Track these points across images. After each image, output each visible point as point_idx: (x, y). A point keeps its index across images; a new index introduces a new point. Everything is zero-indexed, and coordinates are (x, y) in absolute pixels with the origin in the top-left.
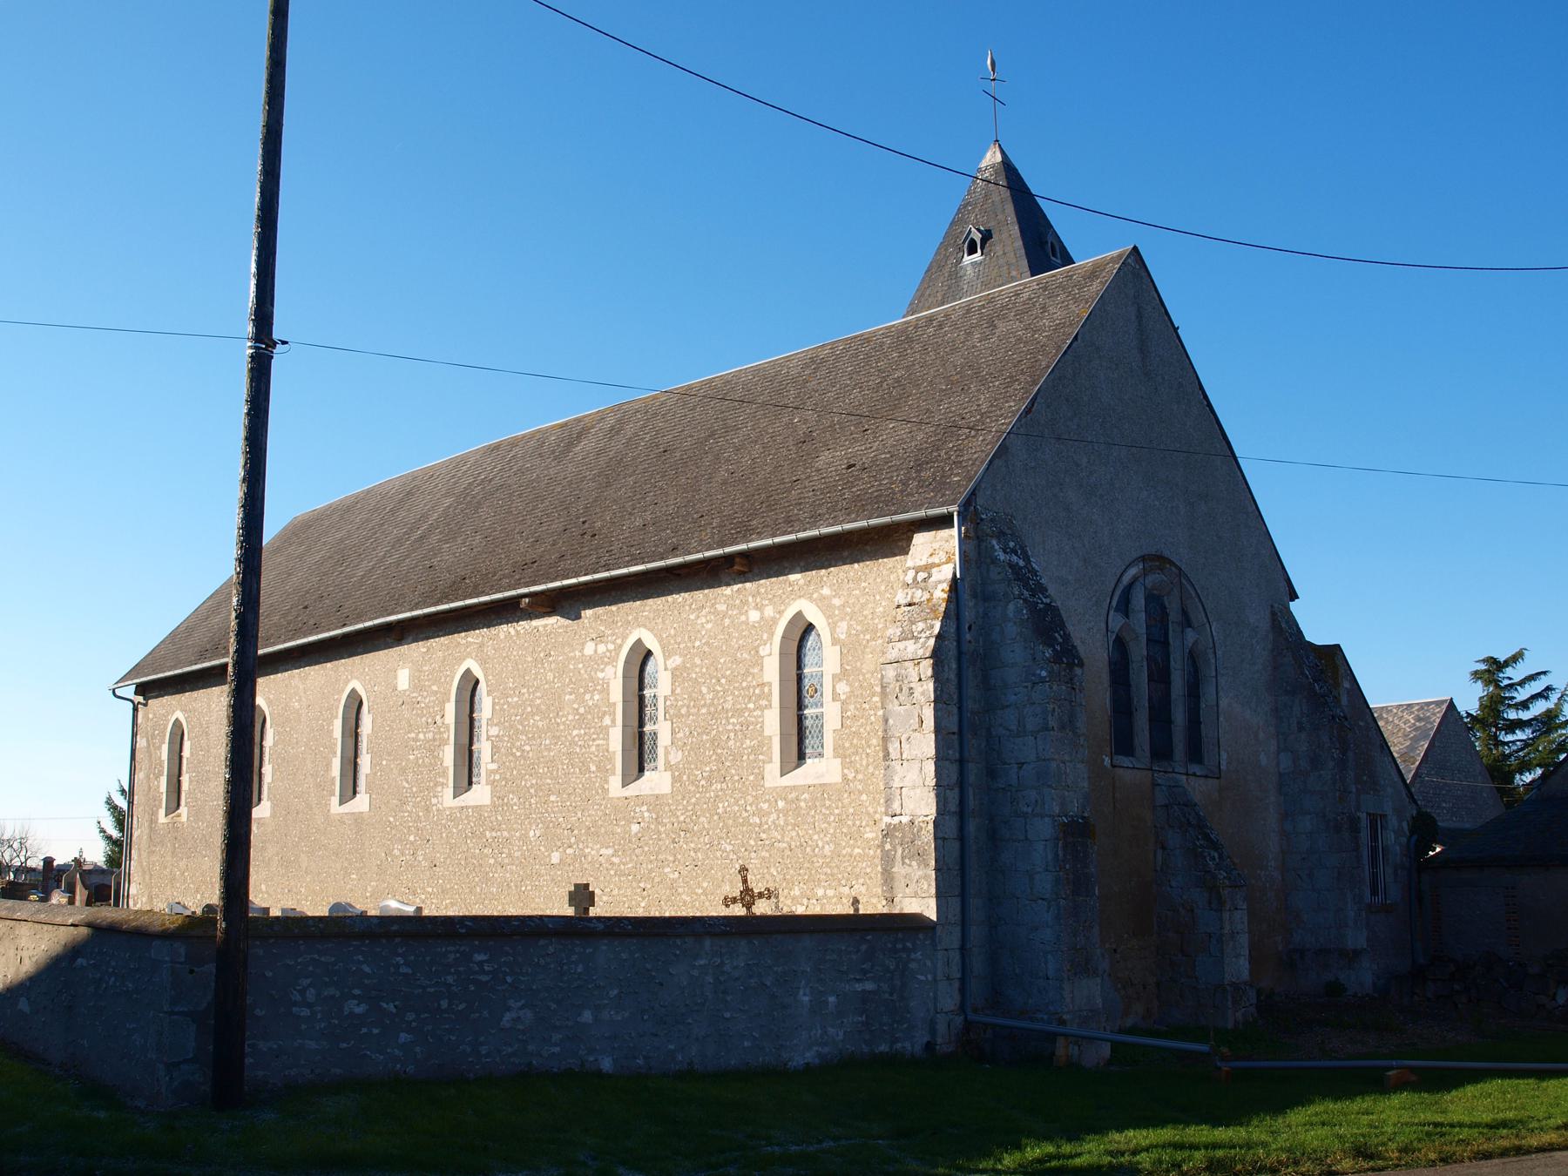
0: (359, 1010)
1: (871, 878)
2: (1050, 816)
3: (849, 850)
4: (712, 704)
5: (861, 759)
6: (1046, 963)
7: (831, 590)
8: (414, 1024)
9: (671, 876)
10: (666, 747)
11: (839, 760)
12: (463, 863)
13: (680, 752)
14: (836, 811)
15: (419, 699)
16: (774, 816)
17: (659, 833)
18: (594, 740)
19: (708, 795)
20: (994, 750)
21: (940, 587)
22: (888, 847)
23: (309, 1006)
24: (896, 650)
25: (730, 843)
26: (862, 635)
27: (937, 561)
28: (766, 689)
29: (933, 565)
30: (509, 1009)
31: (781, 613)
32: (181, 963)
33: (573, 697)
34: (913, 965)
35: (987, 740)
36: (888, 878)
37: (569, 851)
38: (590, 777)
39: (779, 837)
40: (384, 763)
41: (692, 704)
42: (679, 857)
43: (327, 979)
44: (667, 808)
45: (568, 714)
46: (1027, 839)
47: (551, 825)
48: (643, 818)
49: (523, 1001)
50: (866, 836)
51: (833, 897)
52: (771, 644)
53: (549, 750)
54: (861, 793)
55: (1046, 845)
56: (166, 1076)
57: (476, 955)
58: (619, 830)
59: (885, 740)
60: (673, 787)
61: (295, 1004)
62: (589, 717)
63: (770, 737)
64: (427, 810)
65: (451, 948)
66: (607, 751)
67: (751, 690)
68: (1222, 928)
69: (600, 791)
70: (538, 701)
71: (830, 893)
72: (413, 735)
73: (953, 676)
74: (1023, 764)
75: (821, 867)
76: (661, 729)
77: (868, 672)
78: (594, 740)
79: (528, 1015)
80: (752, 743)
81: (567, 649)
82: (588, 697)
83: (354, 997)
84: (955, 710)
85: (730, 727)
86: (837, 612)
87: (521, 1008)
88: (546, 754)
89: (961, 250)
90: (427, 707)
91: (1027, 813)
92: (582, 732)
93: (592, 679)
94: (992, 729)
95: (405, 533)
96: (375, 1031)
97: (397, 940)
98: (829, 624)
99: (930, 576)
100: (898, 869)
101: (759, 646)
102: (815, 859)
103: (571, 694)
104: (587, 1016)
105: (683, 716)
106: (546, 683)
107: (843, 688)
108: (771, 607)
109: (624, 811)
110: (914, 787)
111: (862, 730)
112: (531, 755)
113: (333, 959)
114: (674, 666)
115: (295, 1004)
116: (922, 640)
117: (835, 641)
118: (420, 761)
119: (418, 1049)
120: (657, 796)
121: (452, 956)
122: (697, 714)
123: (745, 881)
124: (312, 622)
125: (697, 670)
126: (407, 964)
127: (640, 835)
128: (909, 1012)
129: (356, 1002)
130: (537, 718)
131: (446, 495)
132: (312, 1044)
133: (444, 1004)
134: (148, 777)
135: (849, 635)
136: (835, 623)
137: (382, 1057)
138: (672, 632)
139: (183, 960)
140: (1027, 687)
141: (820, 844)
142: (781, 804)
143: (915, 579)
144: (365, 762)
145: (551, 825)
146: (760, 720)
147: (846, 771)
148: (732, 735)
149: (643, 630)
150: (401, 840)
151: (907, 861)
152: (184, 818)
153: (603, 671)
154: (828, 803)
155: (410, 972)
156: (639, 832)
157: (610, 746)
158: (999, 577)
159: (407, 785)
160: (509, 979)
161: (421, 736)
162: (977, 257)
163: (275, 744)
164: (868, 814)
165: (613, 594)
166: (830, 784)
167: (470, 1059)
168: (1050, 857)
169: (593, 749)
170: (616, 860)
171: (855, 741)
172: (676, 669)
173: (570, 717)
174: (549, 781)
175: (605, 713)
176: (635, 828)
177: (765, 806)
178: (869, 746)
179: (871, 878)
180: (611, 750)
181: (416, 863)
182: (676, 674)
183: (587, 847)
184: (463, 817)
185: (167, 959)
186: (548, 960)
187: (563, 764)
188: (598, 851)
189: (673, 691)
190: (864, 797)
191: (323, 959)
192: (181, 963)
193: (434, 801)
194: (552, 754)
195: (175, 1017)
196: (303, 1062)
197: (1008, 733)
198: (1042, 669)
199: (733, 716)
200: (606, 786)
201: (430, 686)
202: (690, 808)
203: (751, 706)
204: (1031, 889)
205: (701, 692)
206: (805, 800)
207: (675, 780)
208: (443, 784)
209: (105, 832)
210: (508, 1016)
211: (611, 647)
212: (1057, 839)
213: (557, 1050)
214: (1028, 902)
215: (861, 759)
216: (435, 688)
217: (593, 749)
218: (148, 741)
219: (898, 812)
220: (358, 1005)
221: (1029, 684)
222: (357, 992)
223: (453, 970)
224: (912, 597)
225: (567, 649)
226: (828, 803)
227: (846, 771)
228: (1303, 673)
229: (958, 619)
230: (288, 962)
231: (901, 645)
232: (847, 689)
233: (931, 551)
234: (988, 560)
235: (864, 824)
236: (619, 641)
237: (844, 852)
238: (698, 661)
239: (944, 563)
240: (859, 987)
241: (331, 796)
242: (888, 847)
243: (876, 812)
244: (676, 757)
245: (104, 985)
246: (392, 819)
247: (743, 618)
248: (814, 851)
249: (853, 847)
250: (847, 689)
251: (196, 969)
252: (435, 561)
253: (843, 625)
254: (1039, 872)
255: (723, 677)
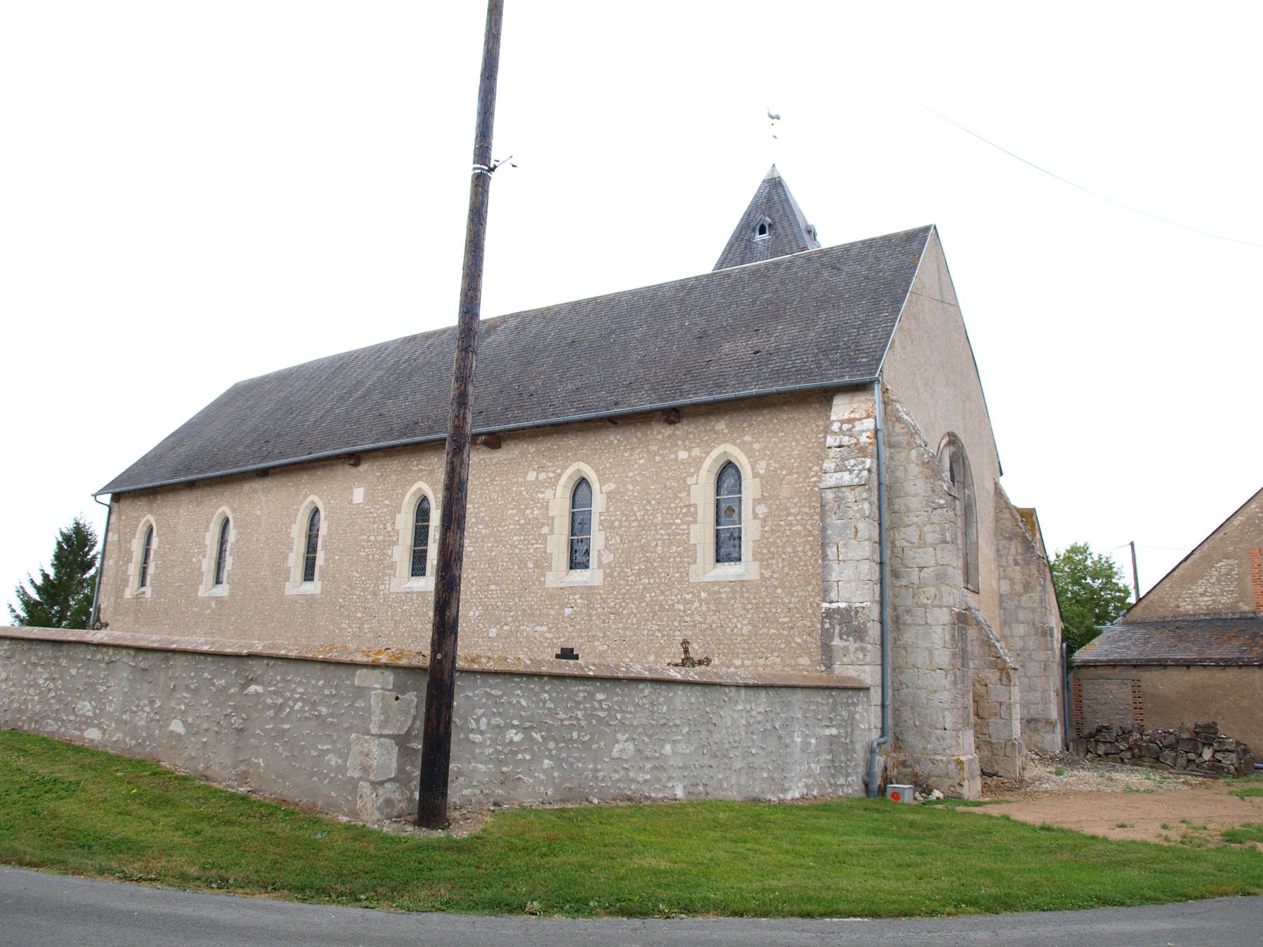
0: (517, 738)
1: (784, 652)
2: (947, 607)
3: (766, 630)
4: (643, 519)
5: (777, 563)
6: (944, 718)
7: (753, 438)
8: (554, 752)
9: (601, 648)
10: (599, 551)
11: (758, 563)
12: (406, 634)
13: (612, 555)
14: (754, 601)
15: (372, 510)
16: (697, 604)
17: (591, 616)
18: (533, 544)
19: (637, 587)
20: (897, 557)
21: (865, 435)
22: (827, 626)
23: (482, 733)
24: (834, 479)
25: (656, 624)
26: (779, 471)
27: (858, 416)
28: (692, 509)
29: (855, 420)
30: (617, 742)
31: (708, 453)
32: (389, 690)
33: (515, 511)
34: (857, 716)
35: (892, 550)
36: (827, 649)
37: (506, 628)
38: (528, 573)
39: (701, 620)
40: (337, 557)
41: (624, 519)
42: (609, 633)
43: (495, 710)
44: (598, 597)
45: (510, 524)
46: (927, 623)
47: (490, 607)
48: (576, 603)
49: (627, 735)
50: (780, 620)
51: (750, 666)
52: (698, 476)
53: (491, 551)
54: (776, 587)
55: (944, 629)
56: (372, 793)
57: (597, 695)
58: (553, 613)
59: (824, 546)
60: (604, 580)
61: (472, 731)
62: (529, 527)
63: (695, 545)
64: (375, 594)
65: (581, 688)
66: (545, 552)
67: (679, 510)
68: (1010, 698)
69: (537, 583)
70: (482, 514)
71: (747, 663)
72: (365, 537)
73: (876, 501)
74: (923, 568)
75: (739, 643)
76: (597, 539)
77: (784, 498)
78: (533, 544)
79: (630, 747)
80: (679, 549)
81: (510, 476)
82: (528, 511)
83: (514, 727)
84: (877, 526)
85: (659, 537)
86: (757, 454)
87: (626, 740)
88: (488, 553)
89: (754, 230)
90: (379, 516)
91: (927, 604)
92: (522, 538)
93: (532, 498)
94: (896, 542)
95: (346, 393)
96: (528, 757)
97: (546, 679)
98: (750, 462)
99: (854, 427)
100: (836, 642)
101: (686, 477)
102: (734, 637)
103: (513, 509)
104: (668, 748)
105: (615, 527)
106: (490, 501)
107: (762, 510)
108: (698, 449)
109: (561, 596)
110: (849, 582)
111: (778, 541)
112: (473, 554)
113: (500, 693)
114: (608, 490)
115: (472, 731)
116: (856, 472)
117: (756, 475)
118: (371, 557)
119: (556, 774)
120: (590, 587)
121: (581, 695)
122: (629, 527)
123: (686, 651)
124: (276, 451)
125: (630, 494)
126: (551, 699)
127: (572, 617)
128: (855, 753)
129: (515, 731)
130: (480, 527)
131: (377, 368)
132: (482, 767)
133: (575, 735)
134: (117, 563)
135: (767, 469)
136: (756, 462)
137: (531, 781)
138: (608, 465)
139: (391, 687)
140: (927, 511)
141: (739, 626)
142: (703, 595)
143: (841, 429)
144: (320, 557)
145: (490, 607)
146: (687, 531)
147: (763, 571)
148: (660, 543)
149: (581, 463)
150: (348, 617)
151: (845, 637)
152: (148, 595)
153: (543, 493)
154: (746, 595)
155: (553, 707)
156: (572, 614)
157: (548, 548)
158: (904, 431)
159: (357, 575)
160: (619, 716)
161: (372, 538)
162: (765, 236)
163: (237, 541)
164: (784, 604)
165: (555, 436)
166: (750, 581)
167: (591, 784)
168: (948, 637)
169: (531, 551)
170: (549, 635)
171: (772, 549)
172: (610, 492)
173: (512, 527)
174: (489, 574)
175: (543, 524)
176: (568, 611)
177: (689, 597)
178: (784, 553)
179: (784, 652)
180: (548, 551)
181: (362, 634)
182: (610, 496)
183: (523, 625)
184: (408, 600)
185: (376, 686)
186: (645, 701)
187: (503, 561)
188: (533, 628)
189: (607, 510)
190: (779, 591)
191: (493, 692)
192: (389, 690)
193: (382, 587)
194: (493, 554)
195: (383, 739)
196: (475, 783)
197: (910, 545)
198: (940, 498)
199: (661, 529)
200: (542, 579)
201: (383, 501)
202: (620, 597)
203: (678, 521)
204: (931, 661)
205: (632, 510)
206: (725, 592)
207: (606, 576)
208: (390, 575)
209: (15, 611)
210: (617, 747)
211: (551, 475)
212: (954, 624)
213: (648, 777)
214: (927, 671)
215: (777, 563)
216: (387, 502)
217: (531, 551)
218: (119, 537)
219: (835, 599)
220: (516, 734)
221: (930, 510)
222: (516, 722)
223: (582, 706)
224: (841, 442)
225: (510, 476)
226: (746, 595)
227: (763, 571)
228: (1018, 525)
229: (878, 459)
230: (468, 693)
231: (838, 475)
232: (766, 510)
233: (852, 409)
234: (894, 419)
235: (779, 610)
236: (559, 471)
237: (761, 632)
238: (630, 487)
239: (864, 418)
240: (827, 732)
241: (286, 581)
242: (827, 626)
243: (789, 603)
244: (608, 558)
245: (288, 710)
246: (341, 600)
247: (673, 456)
248: (732, 631)
249: (769, 628)
250: (766, 510)
251: (400, 696)
252: (384, 411)
253: (763, 463)
254: (938, 649)
255: (653, 499)
